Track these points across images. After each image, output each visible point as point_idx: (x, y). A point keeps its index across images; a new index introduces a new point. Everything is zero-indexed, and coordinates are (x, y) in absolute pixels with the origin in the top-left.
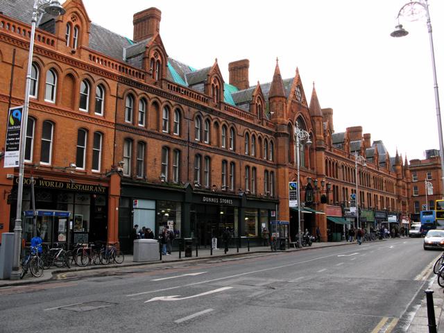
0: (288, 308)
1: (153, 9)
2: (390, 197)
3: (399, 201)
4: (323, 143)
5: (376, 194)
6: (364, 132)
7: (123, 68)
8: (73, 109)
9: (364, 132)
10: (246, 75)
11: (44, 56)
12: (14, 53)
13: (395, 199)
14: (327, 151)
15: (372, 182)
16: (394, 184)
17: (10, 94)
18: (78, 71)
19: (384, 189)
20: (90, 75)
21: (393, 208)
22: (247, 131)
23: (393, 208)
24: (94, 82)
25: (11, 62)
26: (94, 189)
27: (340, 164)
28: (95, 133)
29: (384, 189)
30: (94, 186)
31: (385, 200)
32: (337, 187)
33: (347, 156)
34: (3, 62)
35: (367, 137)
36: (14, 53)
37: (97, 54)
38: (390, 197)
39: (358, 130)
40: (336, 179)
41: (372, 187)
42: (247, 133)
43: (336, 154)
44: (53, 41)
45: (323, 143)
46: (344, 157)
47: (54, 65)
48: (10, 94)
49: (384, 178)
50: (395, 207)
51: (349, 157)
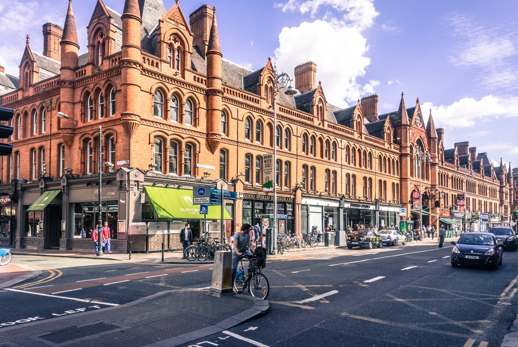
0: (198, 284)
1: (310, 63)
2: (493, 202)
3: (501, 205)
4: (437, 159)
5: (480, 199)
6: (470, 146)
7: (227, 90)
8: (282, 149)
9: (470, 146)
10: (309, 78)
11: (197, 92)
12: (238, 111)
13: (498, 203)
14: (440, 165)
15: (477, 188)
16: (498, 190)
17: (238, 140)
18: (183, 90)
19: (488, 195)
20: (179, 89)
21: (496, 212)
22: (380, 154)
23: (496, 212)
24: (184, 95)
25: (149, 91)
26: (286, 200)
27: (450, 176)
28: (285, 162)
29: (488, 195)
30: (287, 198)
31: (477, 203)
32: (475, 199)
33: (456, 168)
34: (141, 90)
35: (473, 150)
36: (238, 111)
37: (201, 76)
38: (493, 202)
39: (466, 144)
40: (474, 194)
41: (477, 193)
42: (380, 156)
43: (447, 167)
44: (258, 100)
45: (437, 159)
46: (454, 170)
47: (260, 117)
48: (238, 140)
49: (488, 186)
50: (498, 211)
51: (493, 182)
